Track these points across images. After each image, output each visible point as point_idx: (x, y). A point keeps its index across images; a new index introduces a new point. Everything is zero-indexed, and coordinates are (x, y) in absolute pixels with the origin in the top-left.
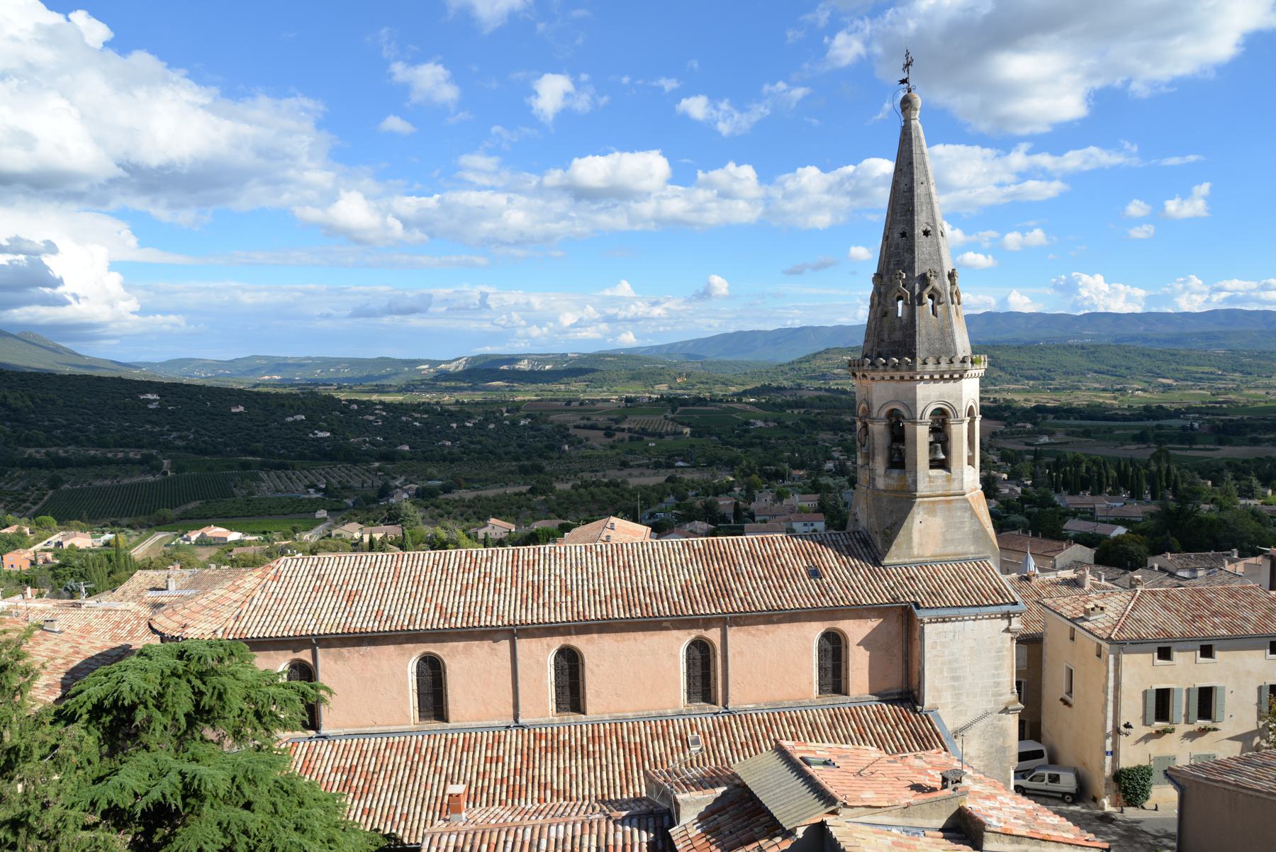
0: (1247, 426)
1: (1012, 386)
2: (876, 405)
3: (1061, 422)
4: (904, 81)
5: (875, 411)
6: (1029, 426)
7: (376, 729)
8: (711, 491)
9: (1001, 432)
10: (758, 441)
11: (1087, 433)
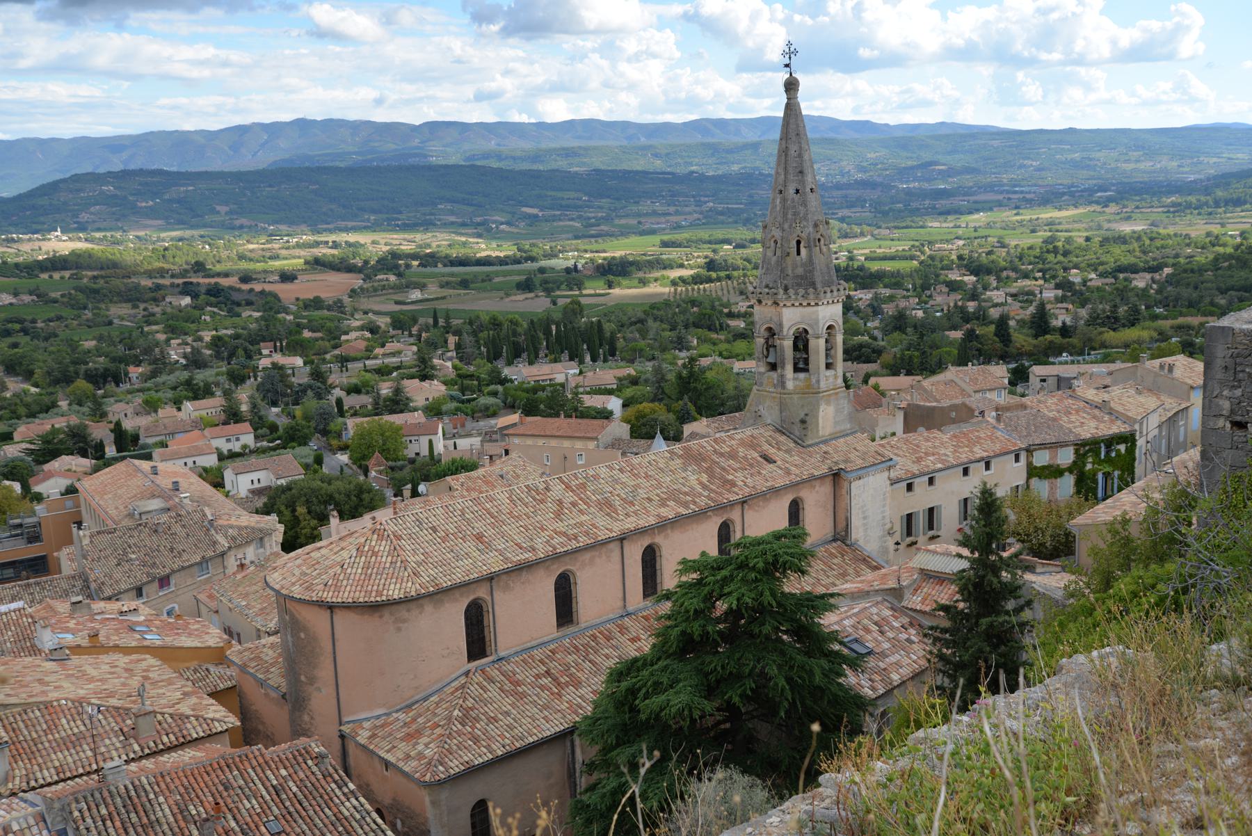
0: (632, 264)
1: (350, 224)
2: (786, 325)
3: (428, 270)
4: (787, 66)
5: (785, 330)
6: (392, 278)
7: (534, 643)
8: (22, 410)
9: (361, 288)
10: (17, 326)
11: (464, 284)
